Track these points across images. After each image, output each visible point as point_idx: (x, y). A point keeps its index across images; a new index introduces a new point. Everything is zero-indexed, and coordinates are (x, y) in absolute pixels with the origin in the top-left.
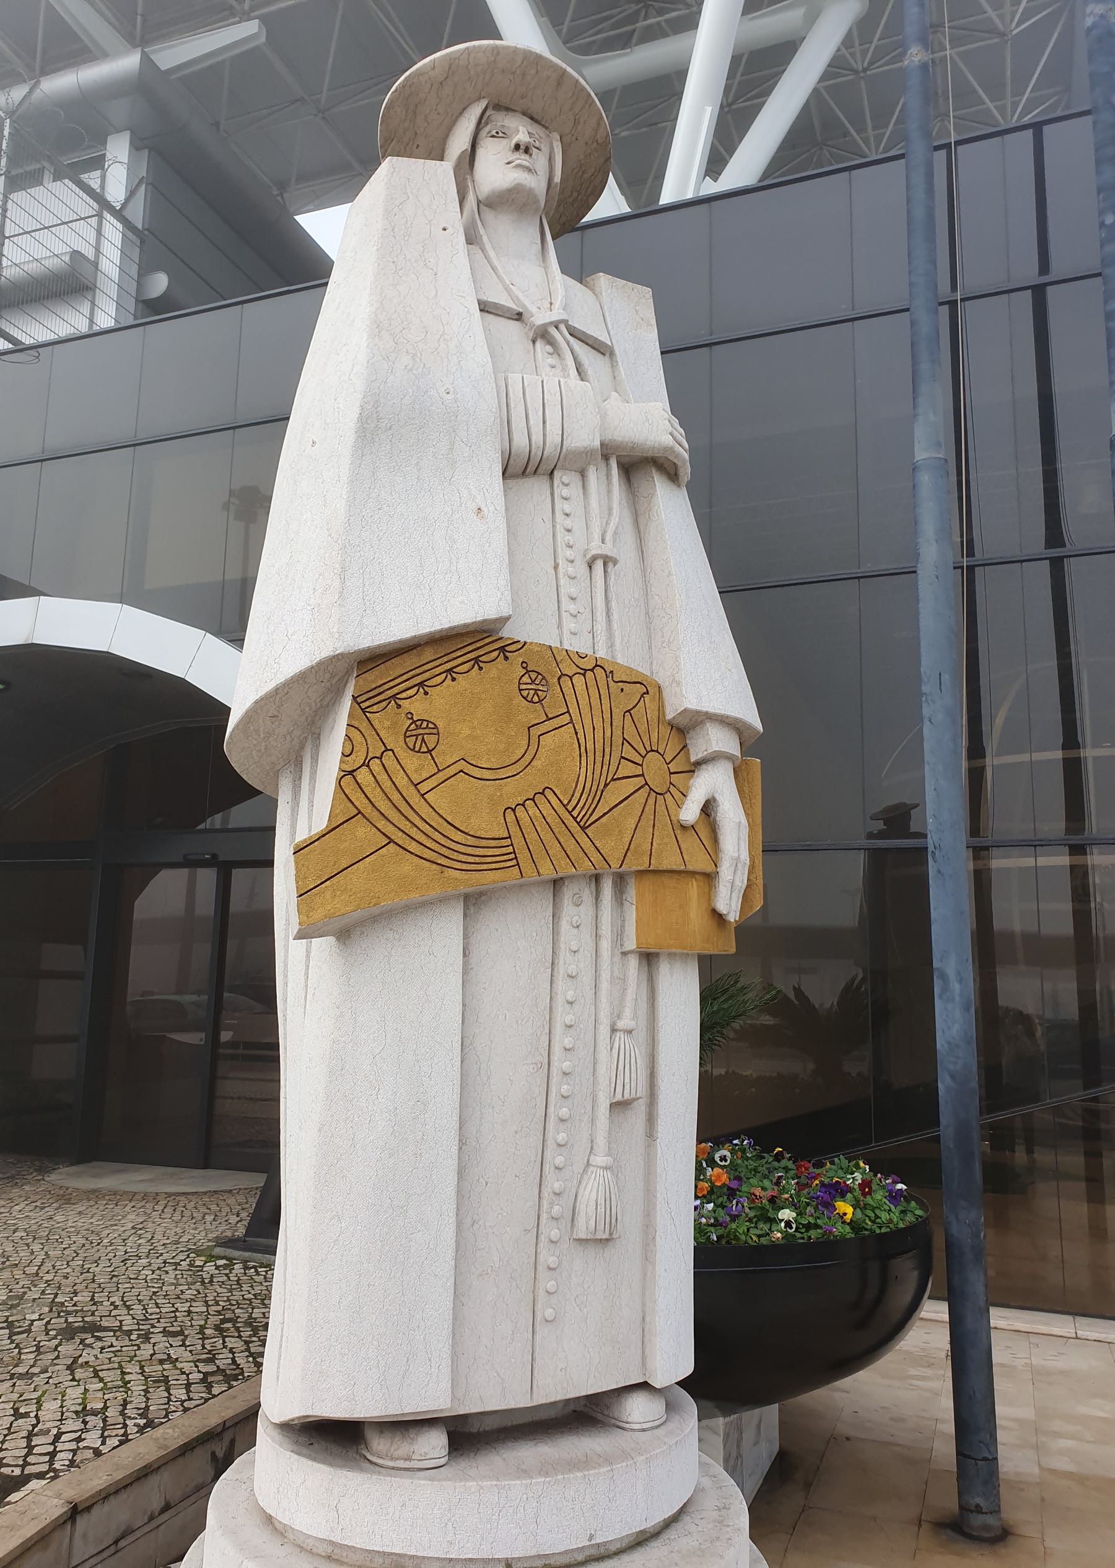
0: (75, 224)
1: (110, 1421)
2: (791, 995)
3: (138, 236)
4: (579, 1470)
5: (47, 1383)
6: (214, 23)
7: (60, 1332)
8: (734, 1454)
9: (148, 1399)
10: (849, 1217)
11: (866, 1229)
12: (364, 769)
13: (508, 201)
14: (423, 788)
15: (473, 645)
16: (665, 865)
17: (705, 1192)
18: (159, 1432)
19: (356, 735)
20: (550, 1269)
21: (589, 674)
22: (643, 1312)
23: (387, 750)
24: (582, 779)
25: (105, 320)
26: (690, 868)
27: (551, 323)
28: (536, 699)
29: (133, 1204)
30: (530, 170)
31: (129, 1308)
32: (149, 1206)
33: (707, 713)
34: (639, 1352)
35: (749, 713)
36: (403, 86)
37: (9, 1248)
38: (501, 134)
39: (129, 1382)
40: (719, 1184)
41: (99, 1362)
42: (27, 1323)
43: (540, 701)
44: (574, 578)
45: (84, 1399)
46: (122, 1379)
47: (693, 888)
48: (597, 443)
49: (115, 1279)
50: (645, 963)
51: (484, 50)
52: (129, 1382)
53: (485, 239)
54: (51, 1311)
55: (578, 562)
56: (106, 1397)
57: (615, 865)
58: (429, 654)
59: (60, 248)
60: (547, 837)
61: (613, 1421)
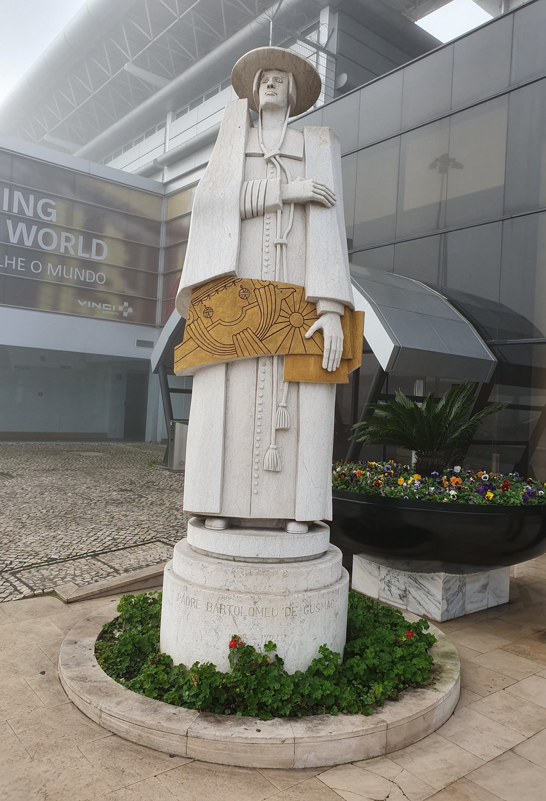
14: (208, 329)
16: (296, 352)
26: (308, 353)
27: (271, 157)
36: (234, 71)
43: (247, 298)
47: (312, 360)
58: (211, 285)
60: (247, 344)
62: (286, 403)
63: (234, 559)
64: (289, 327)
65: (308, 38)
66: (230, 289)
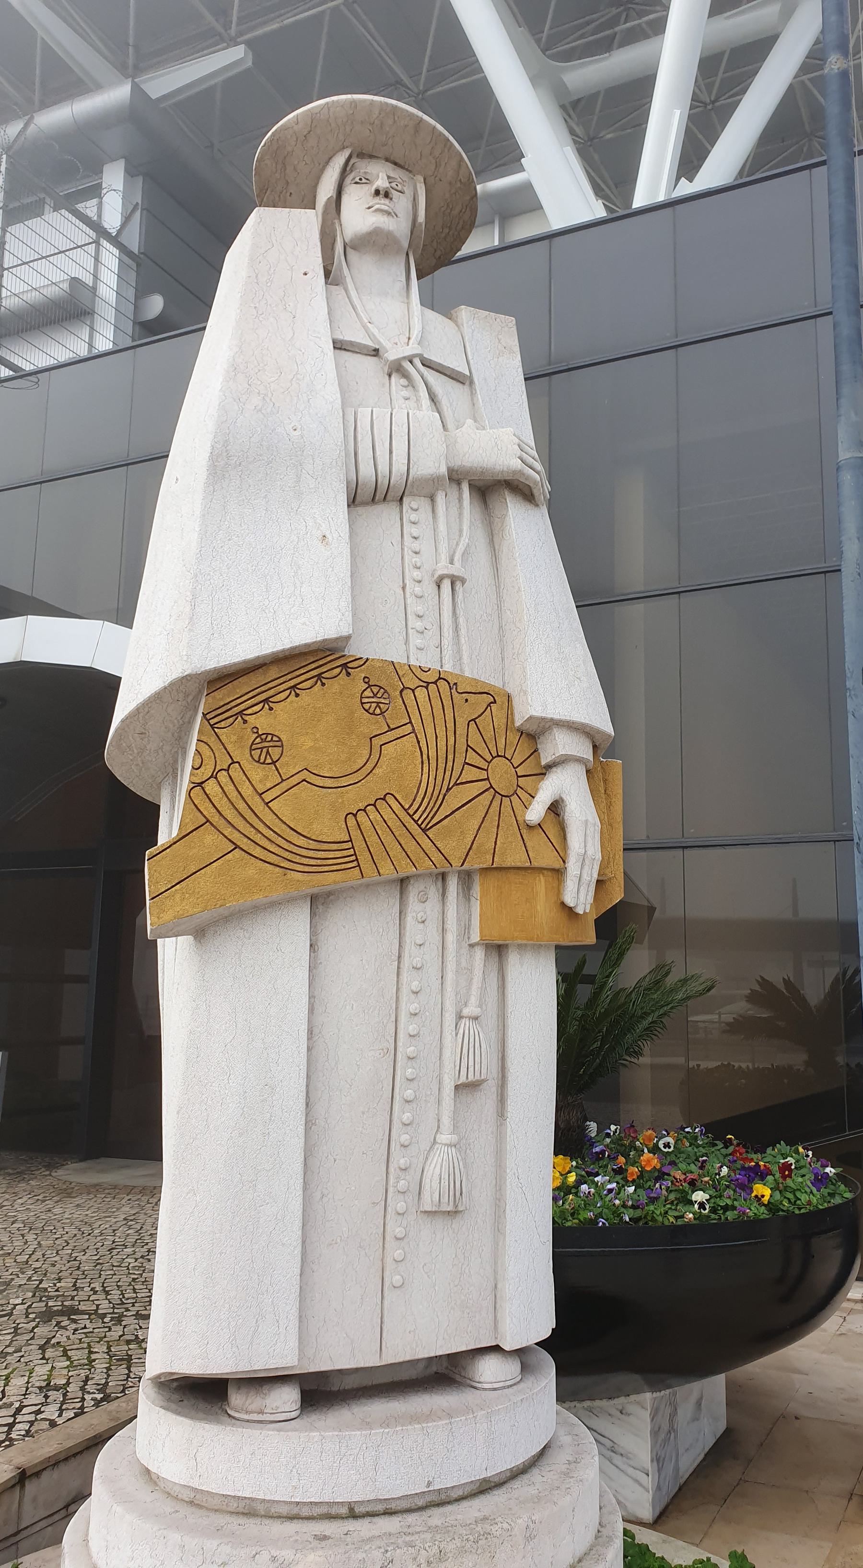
0: (70, 251)
1: (70, 1395)
2: (782, 987)
3: (133, 260)
4: (419, 1423)
5: (19, 1361)
6: (203, 50)
7: (40, 1315)
8: (665, 1427)
9: (109, 1376)
10: (766, 1200)
11: (783, 1211)
12: (213, 780)
13: (374, 243)
14: (268, 797)
15: (319, 661)
17: (635, 1177)
18: (113, 1406)
19: (205, 749)
20: (397, 1239)
21: (432, 687)
22: (496, 1279)
23: (234, 762)
24: (424, 785)
25: (104, 344)
26: (535, 864)
27: (404, 358)
28: (378, 711)
29: (129, 1197)
30: (389, 214)
31: (107, 1293)
32: (145, 1199)
33: (552, 720)
34: (491, 1317)
35: (600, 719)
36: (271, 140)
37: (5, 1238)
38: (364, 181)
39: (94, 1360)
40: (648, 1169)
41: (70, 1342)
42: (10, 1307)
43: (382, 713)
44: (421, 597)
45: (49, 1376)
46: (89, 1358)
47: (541, 884)
48: (443, 470)
49: (99, 1267)
50: (495, 954)
51: (342, 105)
52: (94, 1360)
53: (349, 280)
54: (34, 1296)
55: (426, 582)
56: (70, 1374)
57: (456, 863)
58: (273, 672)
59: (57, 277)
60: (388, 839)
61: (468, 1381)
62: (480, 1006)
63: (351, 1510)
64: (488, 795)
65: (80, 207)
66: (334, 686)
